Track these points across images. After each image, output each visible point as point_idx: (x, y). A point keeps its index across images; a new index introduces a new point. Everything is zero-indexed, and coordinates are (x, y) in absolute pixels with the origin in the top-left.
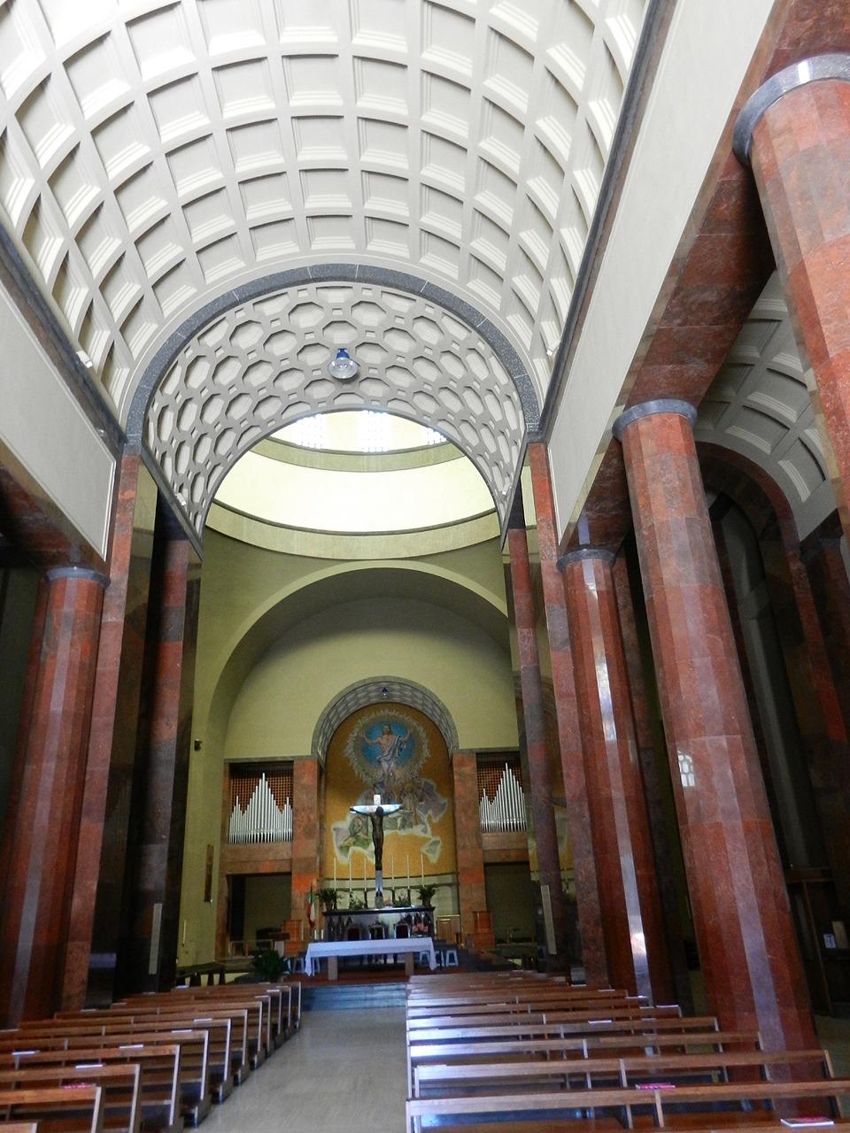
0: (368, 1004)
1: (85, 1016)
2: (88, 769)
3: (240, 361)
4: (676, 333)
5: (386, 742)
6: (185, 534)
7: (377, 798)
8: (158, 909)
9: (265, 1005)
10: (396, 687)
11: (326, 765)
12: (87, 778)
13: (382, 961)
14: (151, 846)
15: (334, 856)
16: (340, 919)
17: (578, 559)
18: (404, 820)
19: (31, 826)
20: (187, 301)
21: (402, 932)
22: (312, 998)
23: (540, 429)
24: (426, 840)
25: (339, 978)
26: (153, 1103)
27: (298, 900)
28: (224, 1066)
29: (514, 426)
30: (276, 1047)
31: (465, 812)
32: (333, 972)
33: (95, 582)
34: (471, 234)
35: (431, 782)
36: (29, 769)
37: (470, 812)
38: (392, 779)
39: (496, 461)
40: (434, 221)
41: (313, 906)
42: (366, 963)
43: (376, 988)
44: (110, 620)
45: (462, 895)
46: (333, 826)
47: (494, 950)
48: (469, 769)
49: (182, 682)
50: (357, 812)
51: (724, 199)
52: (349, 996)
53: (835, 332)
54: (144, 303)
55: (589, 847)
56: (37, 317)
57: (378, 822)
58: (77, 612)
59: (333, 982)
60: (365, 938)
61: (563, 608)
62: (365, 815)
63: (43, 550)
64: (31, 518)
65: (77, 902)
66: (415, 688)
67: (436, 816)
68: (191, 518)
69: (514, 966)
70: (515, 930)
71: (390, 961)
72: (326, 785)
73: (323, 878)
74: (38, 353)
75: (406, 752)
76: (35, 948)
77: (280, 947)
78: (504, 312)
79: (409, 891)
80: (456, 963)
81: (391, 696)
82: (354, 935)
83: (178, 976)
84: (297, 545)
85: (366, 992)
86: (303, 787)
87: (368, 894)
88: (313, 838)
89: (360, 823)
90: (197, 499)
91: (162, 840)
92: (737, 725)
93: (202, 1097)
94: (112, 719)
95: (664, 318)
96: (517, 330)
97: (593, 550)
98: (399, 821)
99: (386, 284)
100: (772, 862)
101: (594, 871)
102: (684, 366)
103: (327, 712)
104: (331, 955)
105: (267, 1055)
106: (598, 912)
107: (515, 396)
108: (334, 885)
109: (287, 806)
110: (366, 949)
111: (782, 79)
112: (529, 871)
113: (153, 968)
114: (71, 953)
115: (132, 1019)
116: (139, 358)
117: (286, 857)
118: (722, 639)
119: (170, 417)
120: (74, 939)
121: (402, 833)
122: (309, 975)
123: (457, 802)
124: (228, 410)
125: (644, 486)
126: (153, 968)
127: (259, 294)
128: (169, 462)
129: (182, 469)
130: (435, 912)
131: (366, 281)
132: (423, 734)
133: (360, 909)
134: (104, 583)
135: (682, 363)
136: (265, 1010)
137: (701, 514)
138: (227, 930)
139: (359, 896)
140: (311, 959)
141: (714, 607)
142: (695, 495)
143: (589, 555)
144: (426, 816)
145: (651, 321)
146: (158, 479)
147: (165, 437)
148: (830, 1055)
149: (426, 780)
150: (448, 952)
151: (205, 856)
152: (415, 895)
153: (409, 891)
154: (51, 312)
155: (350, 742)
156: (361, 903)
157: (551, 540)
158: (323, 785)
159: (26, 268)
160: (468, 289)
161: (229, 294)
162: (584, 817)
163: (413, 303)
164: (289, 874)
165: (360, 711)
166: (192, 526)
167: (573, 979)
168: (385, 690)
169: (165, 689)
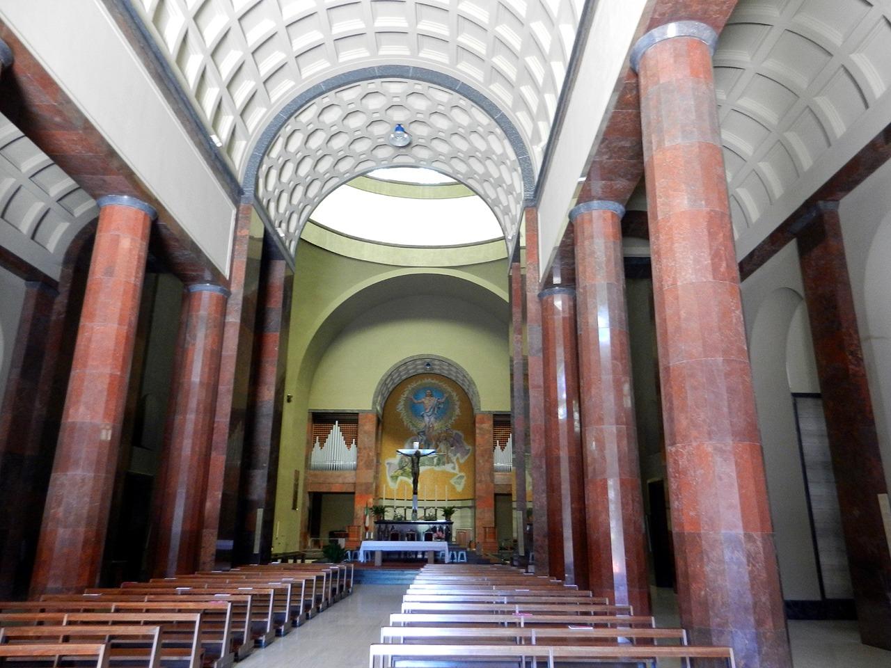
0: (399, 582)
1: (211, 574)
2: (216, 420)
3: (325, 132)
4: (605, 163)
5: (428, 402)
6: (283, 256)
7: (416, 444)
8: (260, 513)
9: (328, 575)
10: (436, 362)
11: (383, 417)
12: (215, 425)
13: (414, 557)
14: (256, 471)
15: (386, 482)
16: (386, 527)
17: (551, 294)
18: (439, 460)
19: (180, 456)
20: (287, 92)
21: (428, 537)
22: (362, 576)
23: (535, 197)
24: (455, 475)
25: (382, 565)
26: (258, 620)
27: (359, 512)
28: (300, 607)
29: (518, 191)
30: (335, 602)
31: (483, 456)
32: (378, 560)
33: (221, 294)
34: (492, 52)
35: (460, 433)
36: (178, 418)
37: (486, 458)
38: (431, 431)
39: (507, 211)
40: (466, 39)
41: (368, 517)
42: (402, 556)
43: (406, 572)
44: (230, 320)
45: (478, 515)
46: (386, 462)
47: (497, 554)
48: (488, 426)
49: (278, 360)
50: (402, 454)
51: (628, 92)
52: (388, 576)
53: (663, 205)
54: (257, 95)
55: (544, 487)
56: (185, 115)
57: (416, 461)
58: (209, 314)
59: (379, 567)
60: (402, 540)
61: (539, 326)
62: (407, 455)
63: (186, 273)
64: (181, 254)
65: (208, 504)
66: (450, 364)
67: (462, 458)
68: (287, 244)
69: (506, 564)
70: (506, 540)
71: (420, 556)
72: (382, 432)
73: (378, 497)
74: (186, 142)
75: (442, 411)
76: (183, 532)
77: (342, 542)
78: (514, 110)
79: (436, 510)
80: (465, 560)
81: (432, 369)
82: (395, 537)
83: (272, 557)
84: (366, 253)
85: (399, 574)
86: (365, 432)
87: (408, 510)
88: (371, 469)
89: (407, 460)
90: (292, 230)
91: (263, 468)
92: (624, 419)
93: (286, 621)
94: (231, 387)
95: (596, 155)
96: (522, 121)
97: (563, 289)
98: (435, 460)
99: (431, 82)
100: (636, 504)
101: (546, 503)
102: (613, 182)
103: (384, 378)
104: (377, 549)
105: (328, 606)
106: (546, 529)
107: (519, 169)
108: (385, 503)
109: (353, 446)
110: (402, 547)
111: (656, 32)
112: (511, 501)
113: (257, 550)
114: (205, 536)
115: (244, 577)
116: (253, 133)
117: (351, 481)
118: (622, 364)
119: (274, 173)
120: (207, 528)
121: (437, 469)
122: (362, 561)
123: (477, 448)
124: (316, 165)
125: (584, 259)
126: (257, 550)
127: (340, 86)
128: (272, 206)
129: (282, 210)
130: (453, 525)
131: (418, 79)
132: (456, 398)
133: (400, 521)
134: (227, 294)
135: (612, 180)
136: (327, 580)
137: (618, 280)
138: (308, 529)
139: (400, 512)
140: (364, 551)
141: (618, 343)
142: (616, 267)
143: (559, 292)
144: (455, 458)
145: (590, 156)
146: (265, 219)
147: (270, 188)
148: (634, 610)
149: (457, 432)
150: (460, 553)
151: (293, 477)
152: (440, 513)
153: (436, 510)
154: (194, 110)
155: (403, 397)
156: (402, 517)
157: (535, 278)
158: (380, 431)
159: (178, 83)
160: (490, 89)
161: (318, 86)
162: (542, 468)
163: (451, 96)
164: (354, 493)
165: (410, 379)
166: (287, 250)
167: (529, 571)
168: (428, 365)
169: (267, 365)
